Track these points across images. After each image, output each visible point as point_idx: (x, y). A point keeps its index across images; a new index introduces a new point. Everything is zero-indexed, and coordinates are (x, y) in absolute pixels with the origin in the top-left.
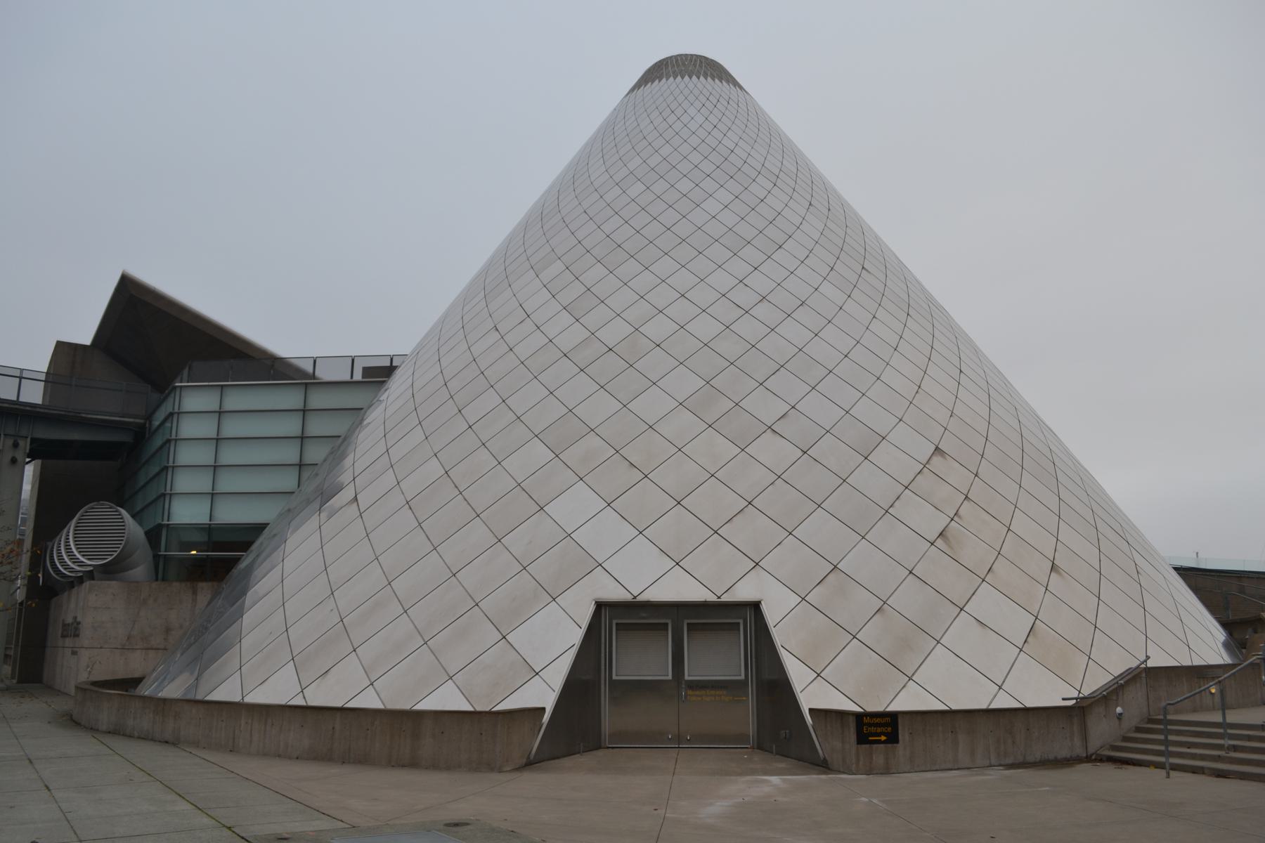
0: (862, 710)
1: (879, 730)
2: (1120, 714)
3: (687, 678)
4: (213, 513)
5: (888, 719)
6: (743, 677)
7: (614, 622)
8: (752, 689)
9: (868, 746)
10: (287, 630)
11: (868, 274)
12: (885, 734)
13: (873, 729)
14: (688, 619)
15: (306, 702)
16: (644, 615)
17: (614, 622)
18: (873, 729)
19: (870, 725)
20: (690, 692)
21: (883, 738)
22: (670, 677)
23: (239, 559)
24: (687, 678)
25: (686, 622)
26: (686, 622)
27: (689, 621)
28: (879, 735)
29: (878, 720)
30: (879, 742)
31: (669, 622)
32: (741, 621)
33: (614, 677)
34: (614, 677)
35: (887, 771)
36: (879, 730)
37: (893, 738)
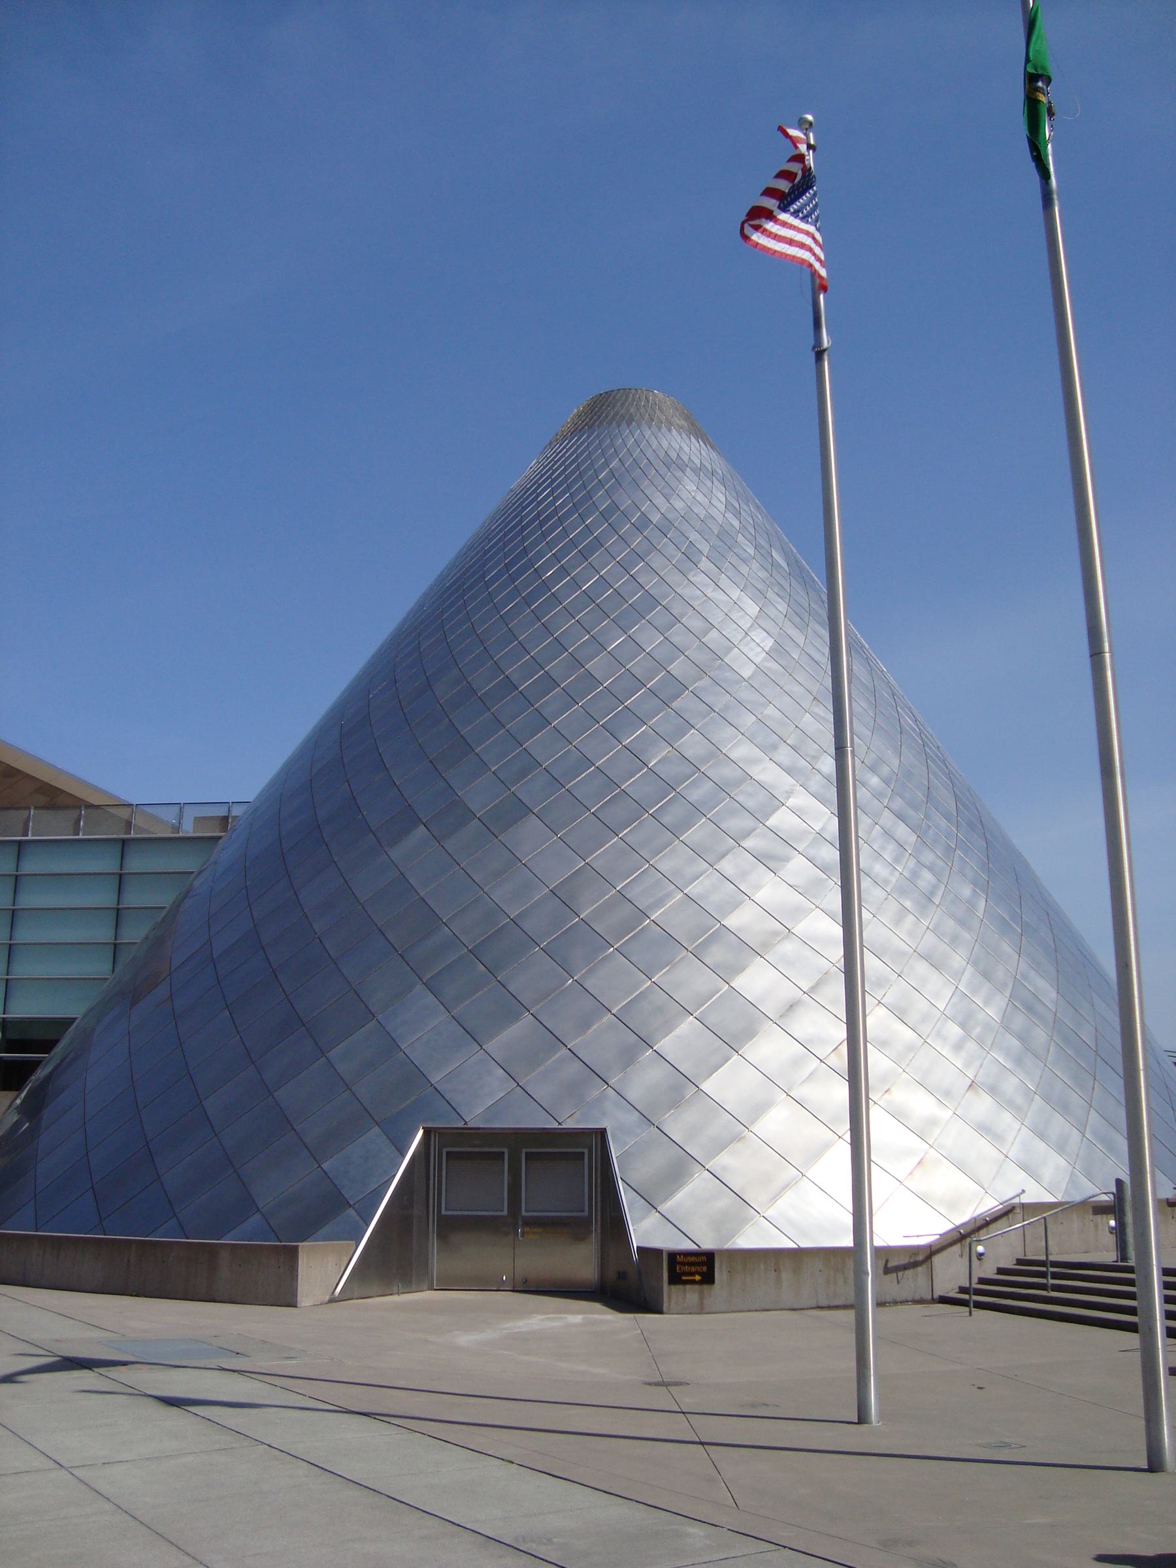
0: (696, 1247)
1: (693, 1269)
2: (981, 1254)
3: (524, 1213)
4: (6, 1009)
5: (704, 1258)
6: (586, 1213)
7: (445, 1150)
8: (595, 1227)
9: (681, 1287)
10: (683, 1413)
11: (81, 1388)
12: (699, 1274)
13: (687, 1268)
14: (526, 1148)
15: (844, 1040)
16: (477, 1142)
17: (445, 1150)
18: (687, 1268)
19: (683, 1264)
20: (527, 1229)
21: (698, 1278)
22: (505, 1213)
23: (41, 1062)
24: (524, 1213)
25: (524, 1150)
26: (524, 1150)
27: (529, 1150)
28: (693, 1274)
29: (692, 1259)
30: (693, 1282)
31: (506, 1150)
32: (586, 1151)
33: (444, 1212)
34: (444, 1212)
35: (701, 1310)
36: (693, 1269)
37: (708, 1279)
